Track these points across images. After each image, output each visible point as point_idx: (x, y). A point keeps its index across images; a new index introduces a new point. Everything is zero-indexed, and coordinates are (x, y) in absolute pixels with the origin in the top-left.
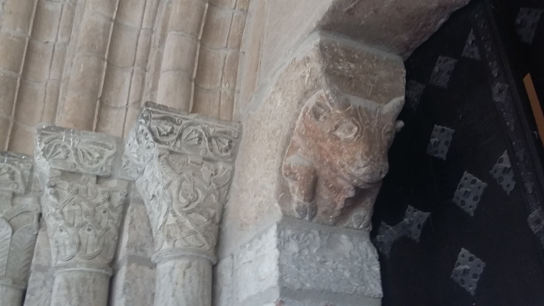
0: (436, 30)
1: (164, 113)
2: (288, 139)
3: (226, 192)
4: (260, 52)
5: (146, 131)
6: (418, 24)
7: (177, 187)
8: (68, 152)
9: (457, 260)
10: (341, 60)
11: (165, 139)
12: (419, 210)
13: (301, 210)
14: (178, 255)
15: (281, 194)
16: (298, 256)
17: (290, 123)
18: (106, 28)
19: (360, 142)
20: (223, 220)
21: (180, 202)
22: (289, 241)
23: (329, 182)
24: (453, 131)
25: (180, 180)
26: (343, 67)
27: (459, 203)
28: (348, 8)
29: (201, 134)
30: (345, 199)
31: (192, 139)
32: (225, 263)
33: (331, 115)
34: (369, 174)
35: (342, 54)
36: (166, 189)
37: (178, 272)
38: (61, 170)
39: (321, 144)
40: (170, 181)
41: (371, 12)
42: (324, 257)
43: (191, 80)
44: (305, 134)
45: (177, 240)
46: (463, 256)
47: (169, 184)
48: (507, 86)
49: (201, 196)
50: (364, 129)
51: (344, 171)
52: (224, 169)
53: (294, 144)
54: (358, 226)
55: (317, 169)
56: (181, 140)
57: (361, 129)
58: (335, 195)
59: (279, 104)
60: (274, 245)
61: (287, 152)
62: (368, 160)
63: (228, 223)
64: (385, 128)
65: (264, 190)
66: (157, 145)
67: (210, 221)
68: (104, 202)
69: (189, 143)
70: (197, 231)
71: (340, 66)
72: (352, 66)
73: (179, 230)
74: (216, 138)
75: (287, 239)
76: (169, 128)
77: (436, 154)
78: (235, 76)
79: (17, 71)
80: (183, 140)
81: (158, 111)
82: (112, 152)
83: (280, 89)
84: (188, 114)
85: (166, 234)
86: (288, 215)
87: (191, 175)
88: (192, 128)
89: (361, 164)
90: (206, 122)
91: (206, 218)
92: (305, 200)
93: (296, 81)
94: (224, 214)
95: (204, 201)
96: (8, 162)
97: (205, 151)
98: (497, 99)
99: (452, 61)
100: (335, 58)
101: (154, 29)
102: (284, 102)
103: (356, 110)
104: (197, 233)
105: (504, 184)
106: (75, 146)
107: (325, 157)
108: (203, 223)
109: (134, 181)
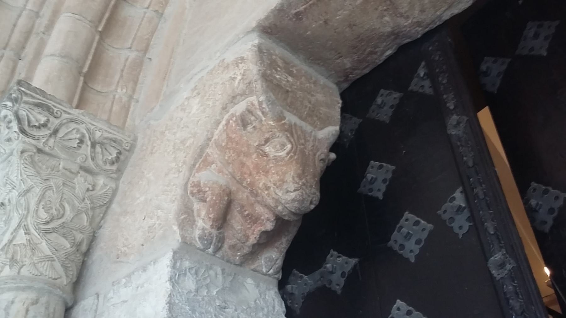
0: (381, 62)
1: (40, 99)
2: (202, 150)
3: (102, 215)
5: (11, 117)
6: (365, 50)
7: (39, 196)
9: (390, 314)
10: (279, 69)
11: (35, 132)
12: (344, 256)
13: (205, 238)
14: (22, 285)
15: (183, 216)
16: (195, 295)
17: (208, 131)
19: (292, 162)
20: (91, 250)
21: (38, 217)
22: (185, 274)
23: (245, 208)
24: (394, 168)
25: (45, 187)
26: (280, 76)
27: (396, 247)
28: (298, 10)
29: (83, 136)
30: (261, 232)
31: (71, 139)
33: (263, 125)
34: (298, 201)
35: (280, 62)
36: (23, 196)
39: (245, 159)
40: (31, 186)
41: (321, 22)
42: (225, 302)
43: (80, 73)
44: (225, 145)
45: (25, 265)
46: (398, 309)
47: (28, 191)
48: (465, 118)
49: (69, 213)
50: (298, 149)
51: (268, 195)
52: (105, 185)
53: (208, 157)
54: (267, 270)
55: (232, 190)
56: (56, 137)
57: (295, 147)
58: (249, 226)
59: (194, 111)
60: (166, 277)
61: (197, 166)
62: (300, 183)
63: (97, 254)
64: (319, 153)
65: (159, 211)
66: (22, 138)
67: (74, 249)
69: (66, 143)
70: (56, 258)
71: (278, 75)
72: (290, 79)
73: (29, 253)
74: (102, 144)
75: (184, 272)
76: (43, 120)
77: (371, 192)
78: (136, 82)
80: (58, 138)
81: (34, 94)
83: (199, 94)
84: (71, 107)
85: (9, 256)
86: (188, 243)
87: (60, 184)
88: (73, 126)
89: (292, 187)
90: (94, 123)
91: (70, 243)
92: (212, 227)
93: (223, 83)
94: (93, 243)
95: (71, 221)
97: (85, 158)
98: (453, 132)
99: (397, 95)
100: (272, 65)
101: (41, 14)
102: (202, 108)
103: (292, 126)
104: (54, 260)
105: (455, 226)
107: (246, 176)
108: (65, 248)
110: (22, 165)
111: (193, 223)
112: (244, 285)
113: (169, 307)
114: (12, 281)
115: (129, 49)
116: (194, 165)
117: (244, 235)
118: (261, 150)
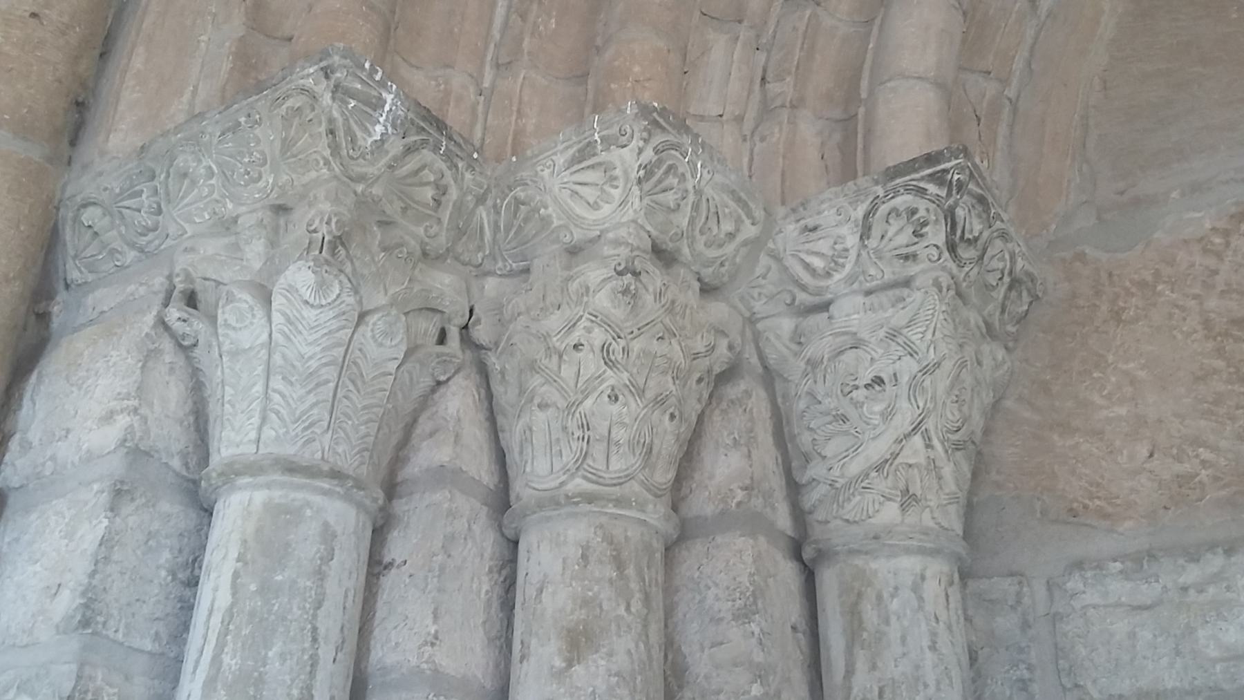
14: (928, 545)
37: (932, 589)
66: (945, 260)
110: (941, 314)
114: (922, 537)
115: (986, 75)
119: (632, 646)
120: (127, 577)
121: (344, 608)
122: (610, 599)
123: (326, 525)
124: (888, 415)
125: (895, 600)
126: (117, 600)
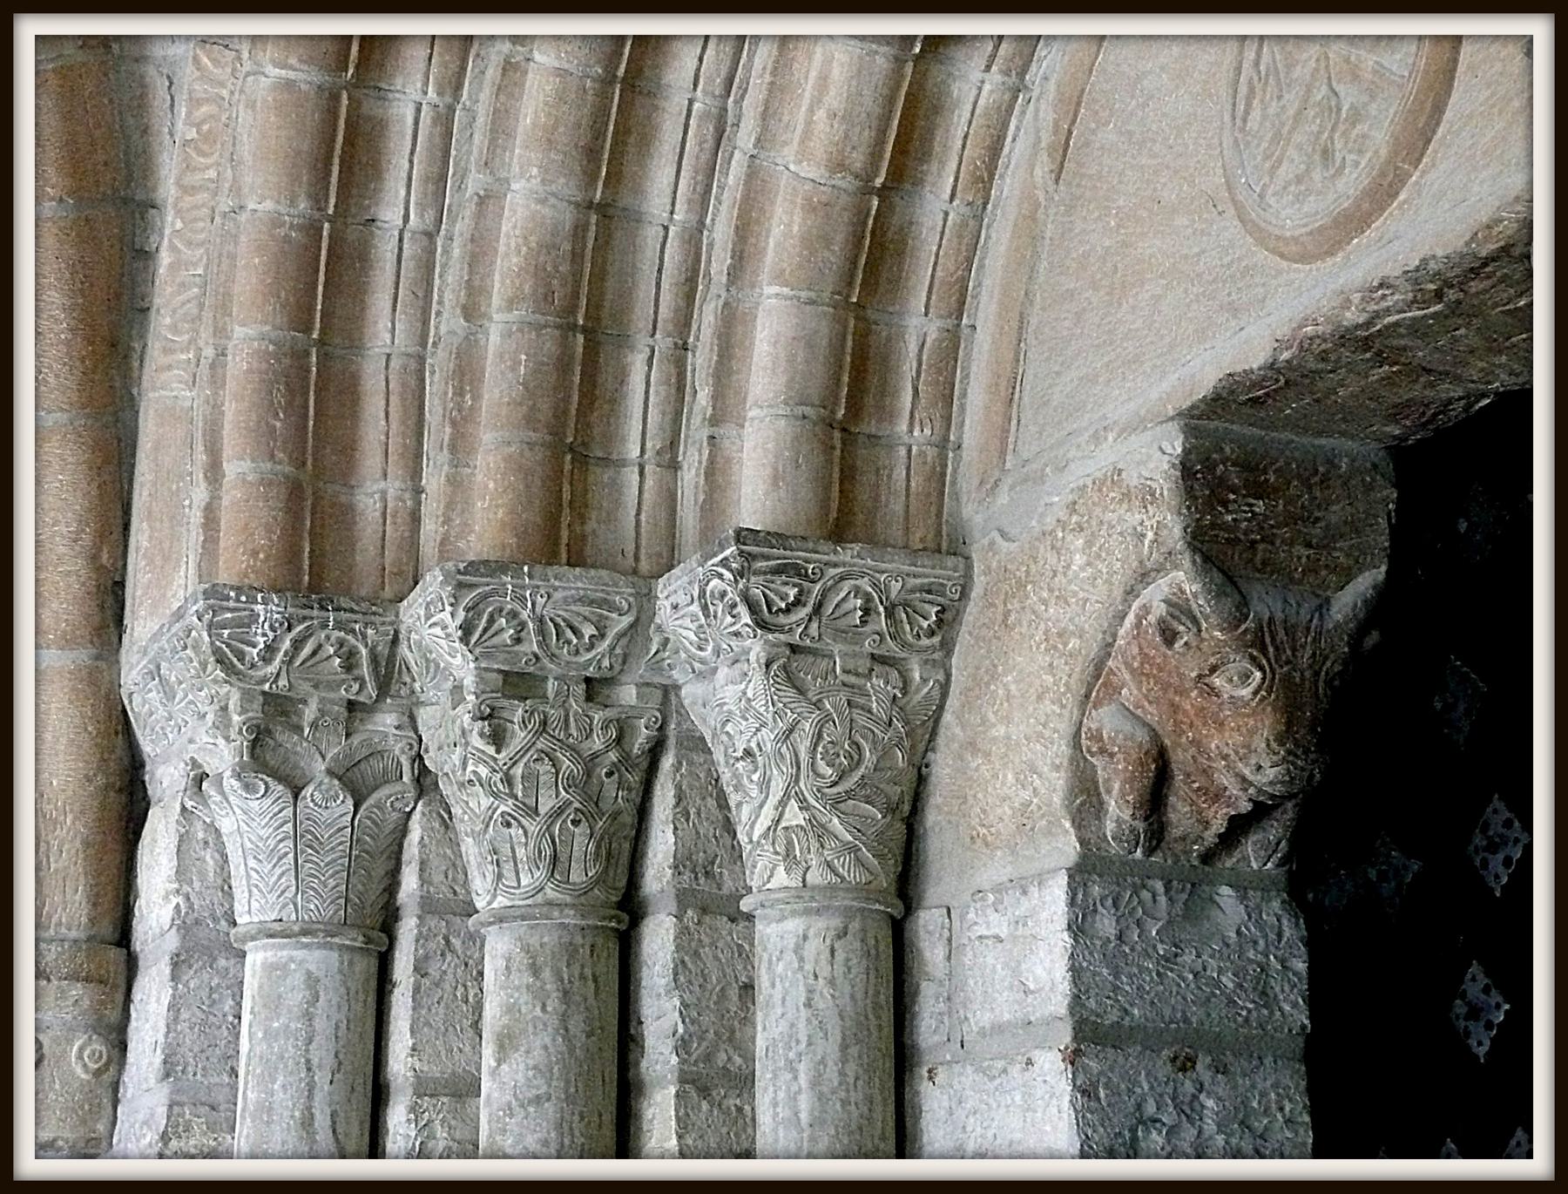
4: (1022, 345)
8: (523, 625)
11: (782, 619)
17: (1104, 633)
18: (579, 230)
26: (1237, 514)
29: (868, 599)
32: (928, 921)
33: (1202, 640)
37: (815, 947)
38: (500, 671)
60: (1061, 920)
63: (934, 817)
68: (607, 749)
72: (1260, 507)
73: (814, 845)
79: (308, 330)
80: (824, 619)
82: (626, 621)
90: (884, 566)
96: (339, 626)
106: (538, 610)
109: (677, 687)
111: (1099, 809)
112: (1215, 902)
113: (1073, 976)
116: (1087, 696)
117: (1198, 821)
118: (1206, 684)
119: (548, 1040)
120: (196, 1030)
121: (337, 1037)
122: (526, 1004)
123: (309, 974)
124: (765, 784)
125: (780, 963)
126: (191, 1051)
